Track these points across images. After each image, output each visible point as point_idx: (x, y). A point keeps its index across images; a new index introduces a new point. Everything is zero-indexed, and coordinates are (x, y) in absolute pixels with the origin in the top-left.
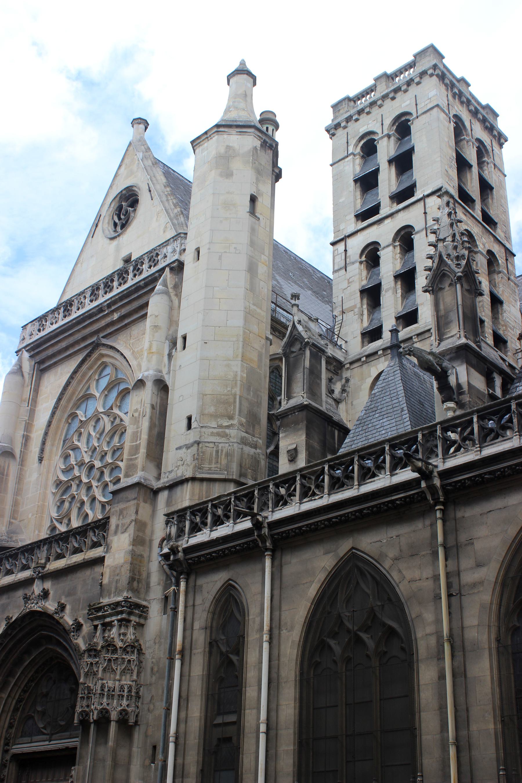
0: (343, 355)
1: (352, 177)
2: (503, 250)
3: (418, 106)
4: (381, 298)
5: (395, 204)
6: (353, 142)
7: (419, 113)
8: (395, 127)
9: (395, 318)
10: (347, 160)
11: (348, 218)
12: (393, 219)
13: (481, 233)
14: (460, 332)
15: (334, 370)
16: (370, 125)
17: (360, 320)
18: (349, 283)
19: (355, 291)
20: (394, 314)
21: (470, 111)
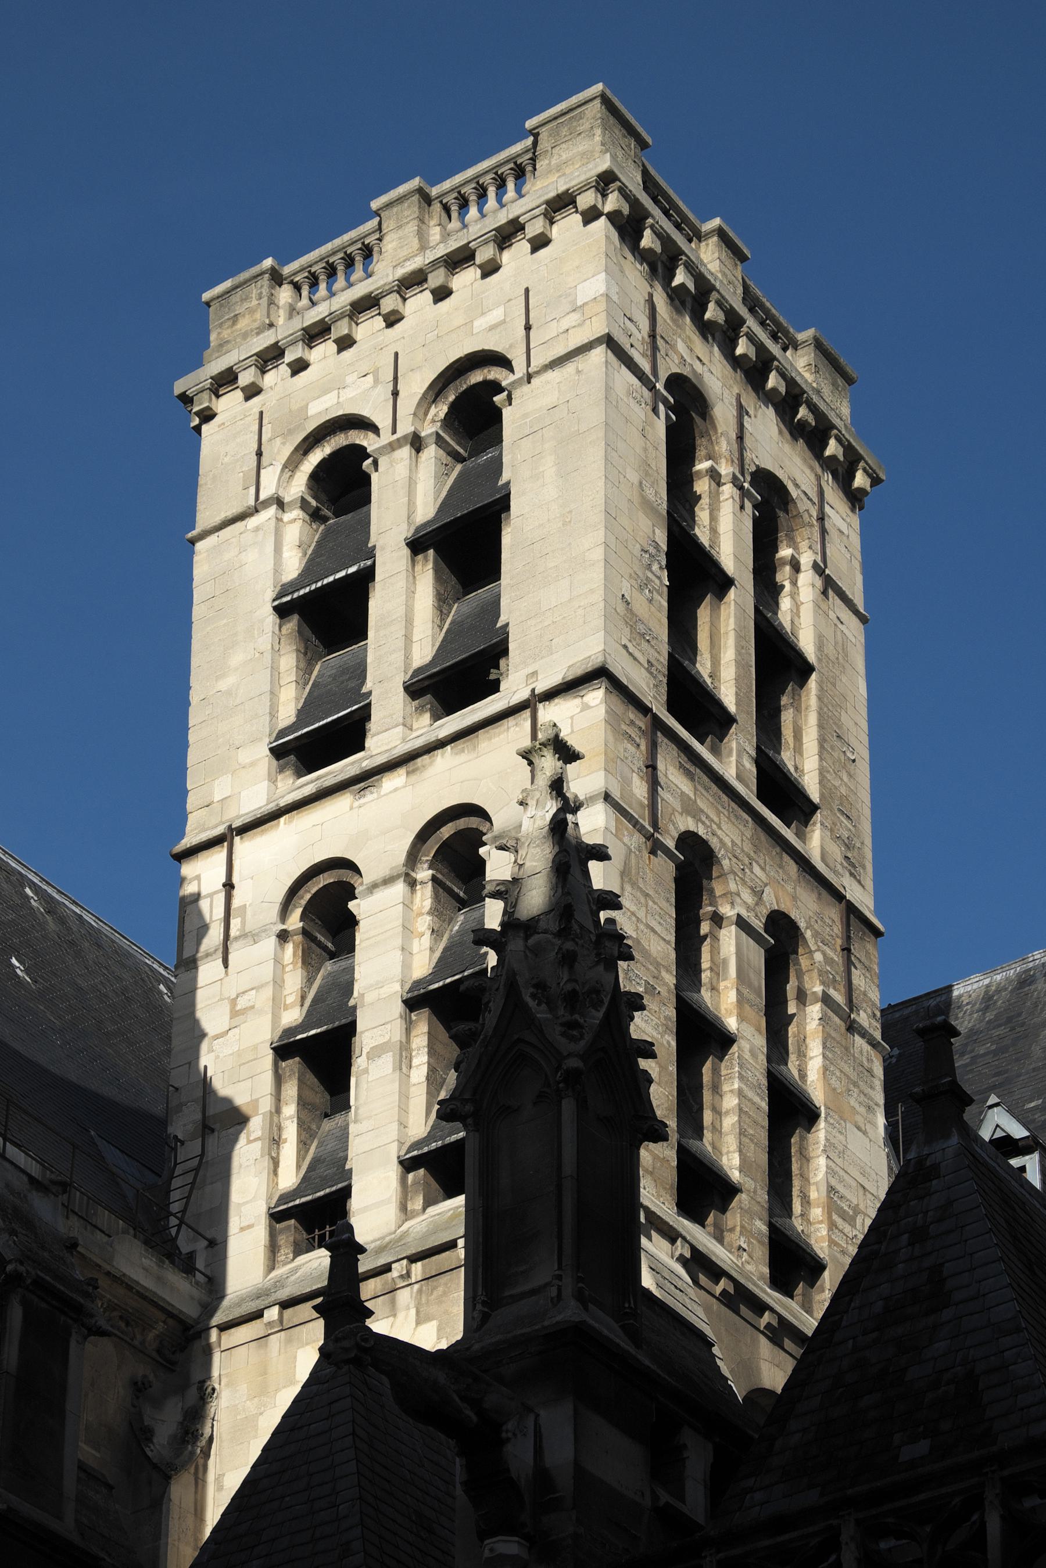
0: (196, 1293)
1: (270, 594)
2: (834, 914)
3: (532, 333)
4: (353, 1080)
5: (427, 717)
6: (280, 450)
7: (536, 363)
8: (441, 410)
9: (401, 1162)
10: (253, 522)
11: (244, 756)
12: (414, 778)
13: (748, 847)
14: (559, 1277)
15: (158, 1351)
16: (347, 394)
17: (266, 1162)
18: (234, 1013)
19: (255, 1048)
20: (395, 1145)
21: (736, 362)
